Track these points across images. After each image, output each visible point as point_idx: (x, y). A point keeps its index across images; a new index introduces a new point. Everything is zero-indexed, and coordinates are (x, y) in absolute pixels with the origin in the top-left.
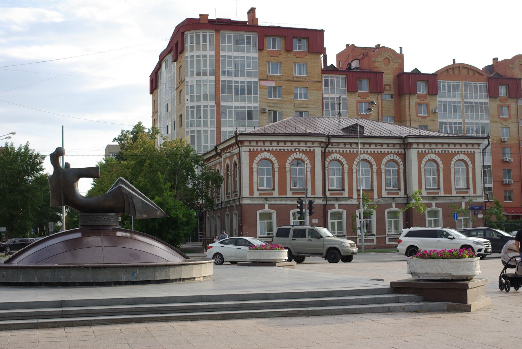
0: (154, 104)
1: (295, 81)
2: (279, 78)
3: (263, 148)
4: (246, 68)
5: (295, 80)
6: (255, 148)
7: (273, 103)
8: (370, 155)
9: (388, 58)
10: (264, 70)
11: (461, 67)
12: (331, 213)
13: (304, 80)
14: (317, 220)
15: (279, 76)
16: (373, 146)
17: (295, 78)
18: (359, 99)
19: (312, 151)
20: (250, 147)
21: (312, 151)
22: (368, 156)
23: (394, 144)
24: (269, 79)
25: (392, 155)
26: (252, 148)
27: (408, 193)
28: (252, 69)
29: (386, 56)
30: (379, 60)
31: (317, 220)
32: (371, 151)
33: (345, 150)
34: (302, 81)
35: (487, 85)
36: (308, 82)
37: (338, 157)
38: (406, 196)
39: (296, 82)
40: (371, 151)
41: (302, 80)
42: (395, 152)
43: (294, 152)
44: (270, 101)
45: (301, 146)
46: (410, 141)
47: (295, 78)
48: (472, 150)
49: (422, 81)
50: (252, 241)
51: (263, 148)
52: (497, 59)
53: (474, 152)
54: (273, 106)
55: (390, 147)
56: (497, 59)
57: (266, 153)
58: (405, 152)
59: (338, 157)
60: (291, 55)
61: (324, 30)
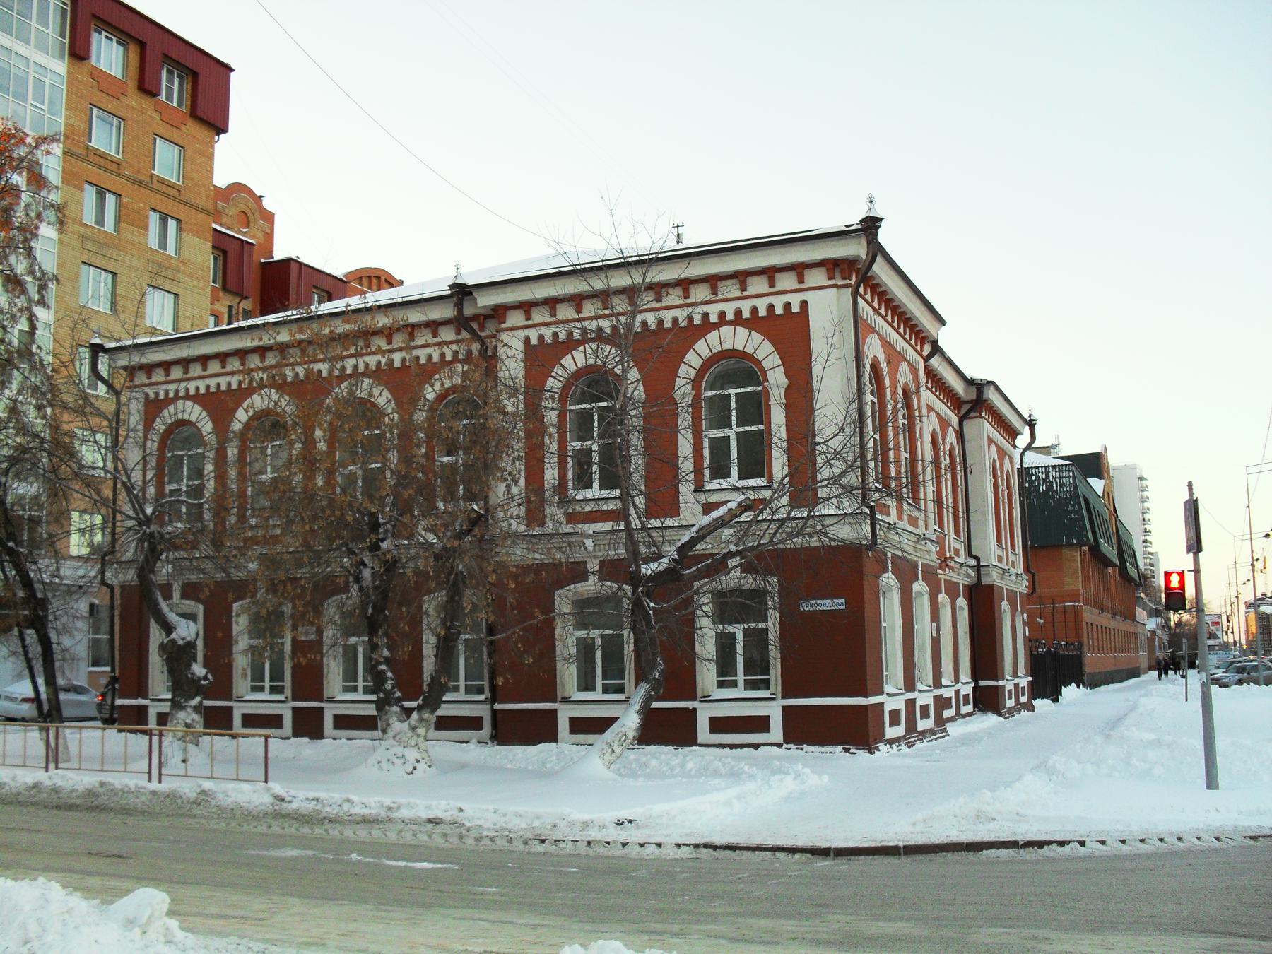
0: (793, 851)
1: (154, 191)
2: (116, 165)
3: (713, 311)
4: (30, 101)
6: (547, 333)
8: (750, 329)
10: (79, 126)
11: (383, 278)
13: (175, 193)
15: (118, 161)
16: (758, 285)
19: (796, 308)
20: (527, 332)
21: (796, 308)
22: (742, 332)
25: (726, 330)
26: (533, 336)
28: (46, 109)
29: (244, 208)
32: (754, 310)
33: (778, 303)
34: (170, 197)
36: (185, 203)
37: (741, 339)
38: (973, 562)
39: (157, 196)
40: (754, 310)
42: (738, 313)
43: (716, 326)
45: (211, 372)
47: (155, 180)
48: (795, 300)
50: (156, 706)
51: (713, 311)
53: (804, 304)
54: (95, 249)
55: (665, 303)
59: (741, 339)
60: (145, 103)
61: (233, 67)
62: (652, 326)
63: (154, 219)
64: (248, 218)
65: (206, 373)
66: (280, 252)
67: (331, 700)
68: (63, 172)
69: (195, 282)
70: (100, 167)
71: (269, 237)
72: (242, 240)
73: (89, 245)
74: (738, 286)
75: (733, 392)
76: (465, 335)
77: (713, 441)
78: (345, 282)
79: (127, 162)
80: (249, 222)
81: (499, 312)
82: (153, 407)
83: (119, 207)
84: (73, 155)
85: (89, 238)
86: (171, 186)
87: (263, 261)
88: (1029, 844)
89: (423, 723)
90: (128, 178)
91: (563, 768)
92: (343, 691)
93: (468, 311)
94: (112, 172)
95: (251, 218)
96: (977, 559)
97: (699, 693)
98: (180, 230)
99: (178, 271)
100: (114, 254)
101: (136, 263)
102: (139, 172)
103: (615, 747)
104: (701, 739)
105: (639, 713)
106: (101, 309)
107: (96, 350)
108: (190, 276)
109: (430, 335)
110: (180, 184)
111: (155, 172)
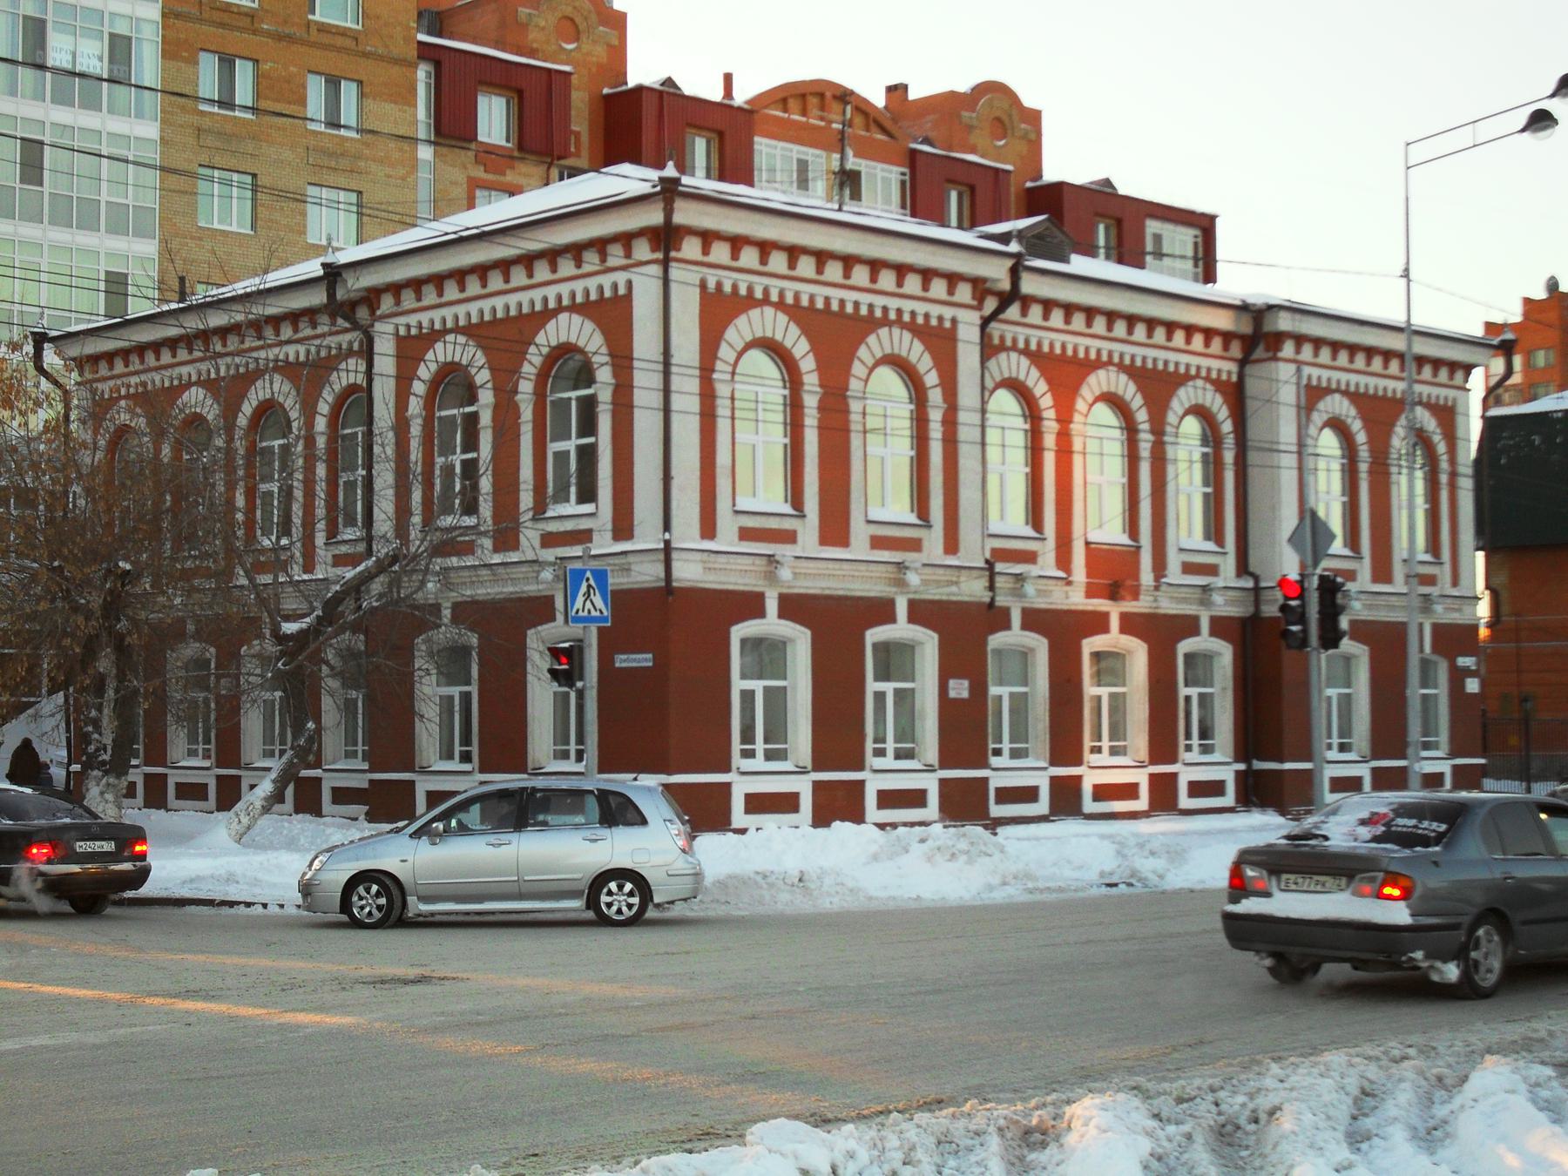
2: (249, 19)
5: (312, 39)
7: (220, 134)
9: (572, 20)
11: (828, 94)
12: (744, 642)
13: (349, 43)
14: (966, 683)
17: (313, 31)
18: (479, 173)
23: (1209, 333)
24: (206, 15)
27: (1254, 566)
29: (569, 11)
30: (543, 23)
31: (966, 683)
34: (340, 50)
35: (907, 178)
36: (366, 55)
38: (1250, 584)
41: (339, 41)
44: (206, 123)
46: (1284, 323)
47: (313, 31)
49: (700, 128)
52: (905, 87)
54: (218, 144)
56: (905, 87)
57: (769, 311)
58: (1241, 376)
62: (291, 358)
63: (316, 90)
64: (576, 26)
65: (533, 281)
66: (642, 71)
67: (424, 771)
68: (163, 42)
69: (388, 170)
70: (222, 25)
71: (618, 54)
72: (549, 70)
73: (210, 141)
74: (413, 295)
75: (573, 394)
76: (342, 323)
77: (556, 454)
78: (750, 112)
79: (267, 11)
80: (578, 32)
81: (372, 297)
82: (411, 349)
83: (258, 78)
84: (178, 16)
85: (209, 131)
86: (343, 32)
87: (606, 91)
88: (223, 903)
89: (111, 789)
90: (268, 34)
91: (1139, 880)
92: (555, 758)
93: (340, 294)
94: (242, 30)
95: (582, 26)
96: (1256, 578)
97: (530, 765)
98: (362, 95)
99: (358, 157)
100: (250, 147)
101: (287, 155)
102: (286, 22)
103: (242, 817)
104: (736, 824)
105: (274, 781)
106: (234, 228)
107: (40, 339)
108: (381, 161)
109: (572, 263)
110: (360, 27)
111: (317, 17)
